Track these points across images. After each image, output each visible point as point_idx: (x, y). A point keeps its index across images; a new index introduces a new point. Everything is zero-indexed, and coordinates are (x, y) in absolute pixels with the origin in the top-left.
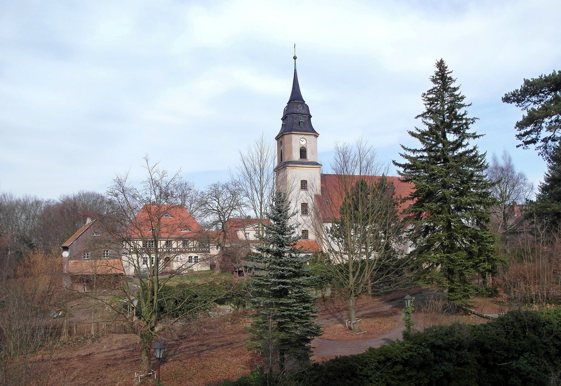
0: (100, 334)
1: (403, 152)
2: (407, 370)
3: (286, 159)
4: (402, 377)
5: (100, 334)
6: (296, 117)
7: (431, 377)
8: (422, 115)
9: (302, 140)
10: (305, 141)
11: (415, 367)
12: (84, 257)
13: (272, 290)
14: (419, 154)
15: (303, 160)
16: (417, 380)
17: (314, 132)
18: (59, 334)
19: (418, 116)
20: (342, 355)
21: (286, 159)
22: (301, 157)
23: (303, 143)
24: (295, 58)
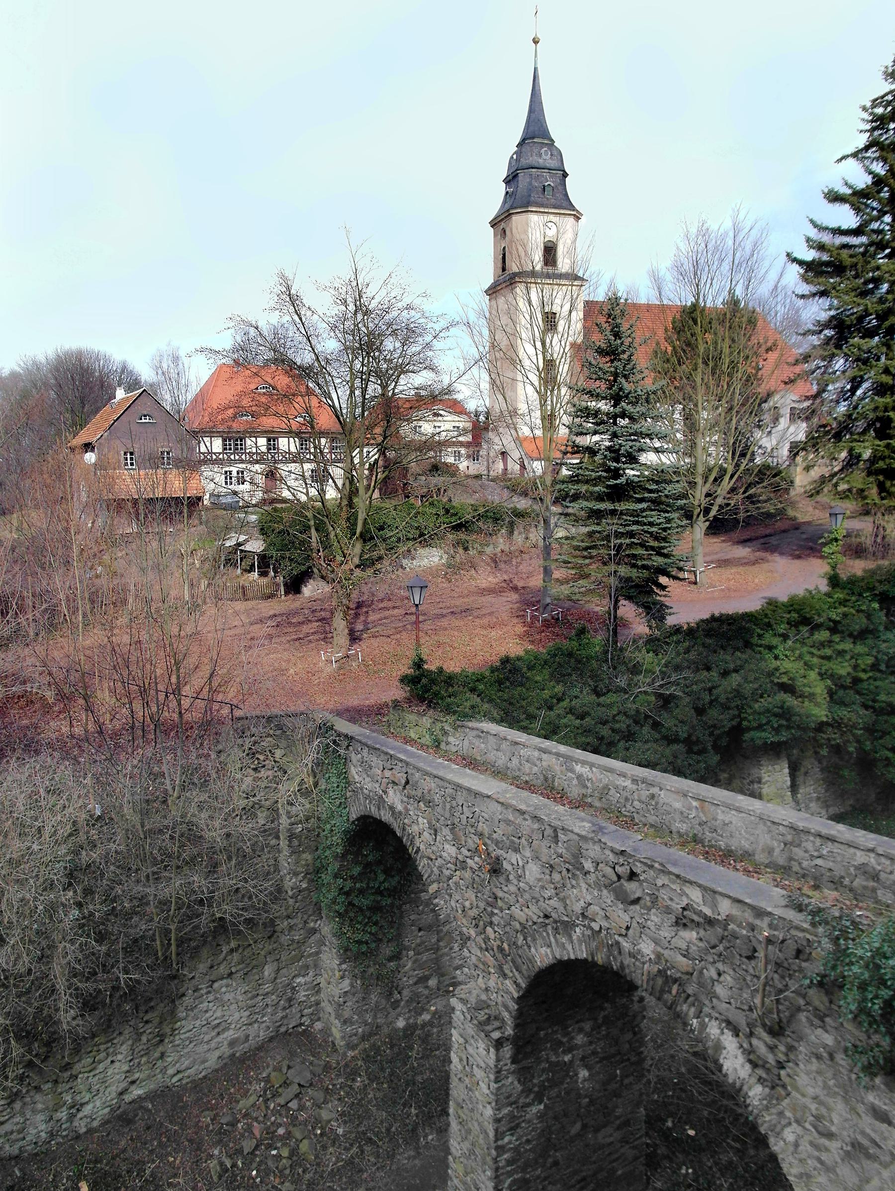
1: (813, 233)
3: (514, 268)
4: (828, 652)
6: (535, 178)
7: (878, 652)
8: (855, 155)
9: (549, 224)
10: (554, 228)
11: (851, 635)
12: (126, 464)
13: (608, 487)
14: (840, 240)
15: (550, 270)
16: (852, 658)
19: (844, 158)
20: (723, 612)
21: (514, 268)
22: (546, 263)
23: (551, 233)
24: (536, 41)
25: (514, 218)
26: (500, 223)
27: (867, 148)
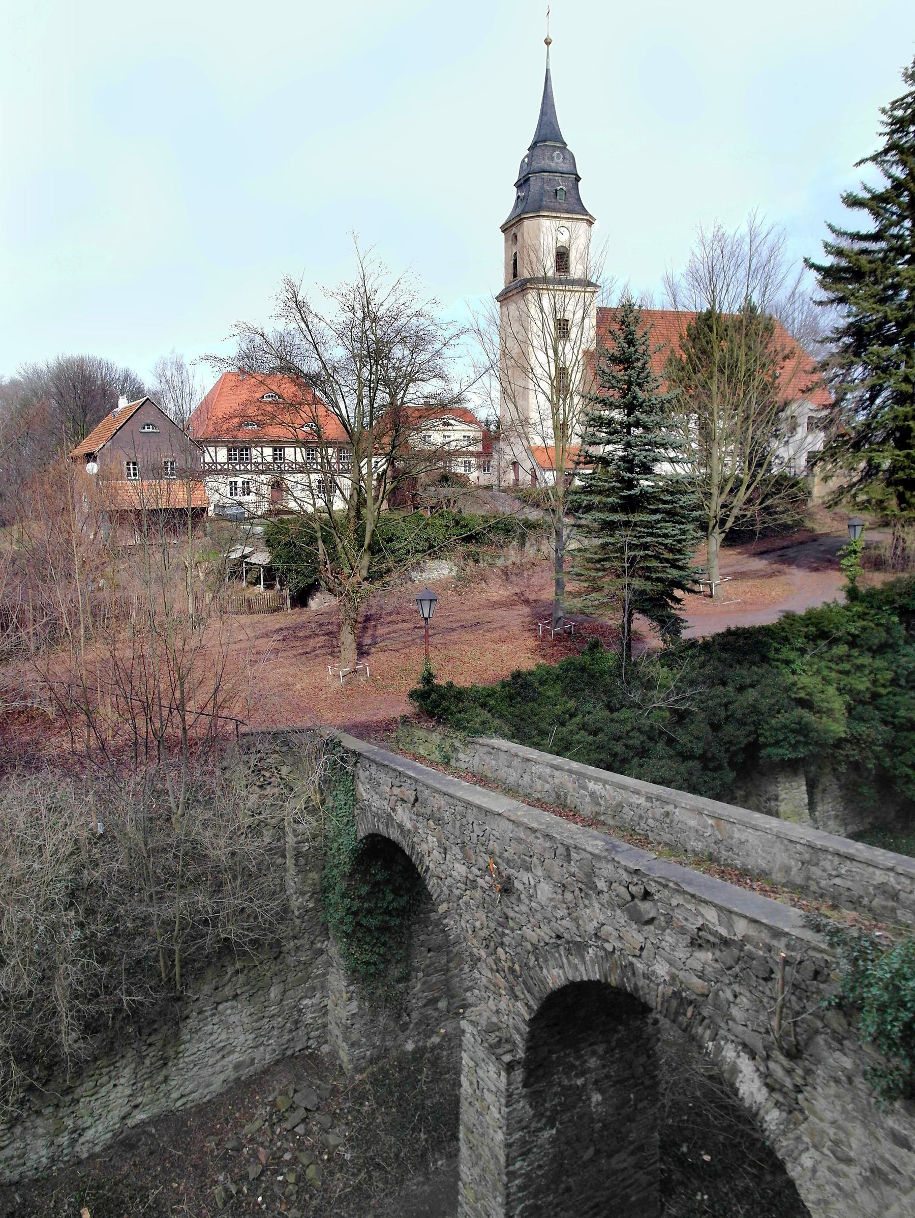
0: (204, 615)
1: (831, 238)
2: (856, 654)
3: (525, 274)
4: (846, 666)
5: (204, 615)
6: (547, 182)
7: (898, 667)
8: (874, 159)
9: (562, 229)
10: (566, 233)
13: (621, 498)
15: (563, 276)
17: (587, 214)
18: (127, 615)
19: (863, 161)
20: (740, 625)
21: (525, 274)
23: (563, 239)
24: (548, 42)
25: (526, 223)
26: (511, 228)
27: (886, 152)
